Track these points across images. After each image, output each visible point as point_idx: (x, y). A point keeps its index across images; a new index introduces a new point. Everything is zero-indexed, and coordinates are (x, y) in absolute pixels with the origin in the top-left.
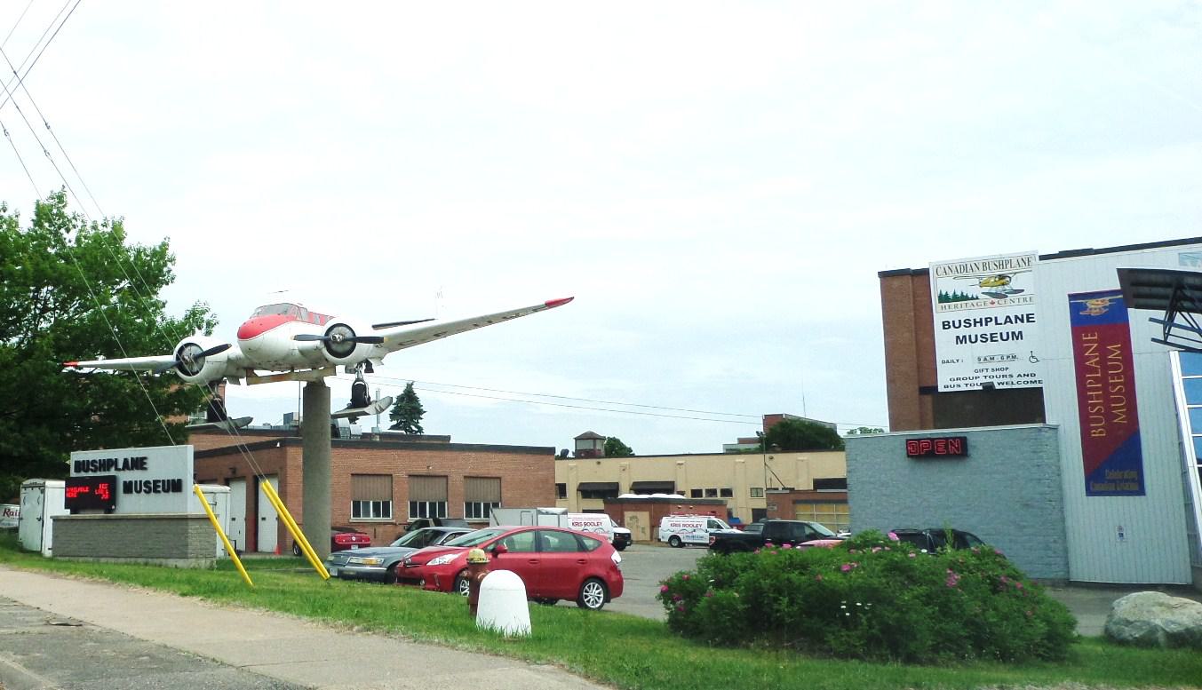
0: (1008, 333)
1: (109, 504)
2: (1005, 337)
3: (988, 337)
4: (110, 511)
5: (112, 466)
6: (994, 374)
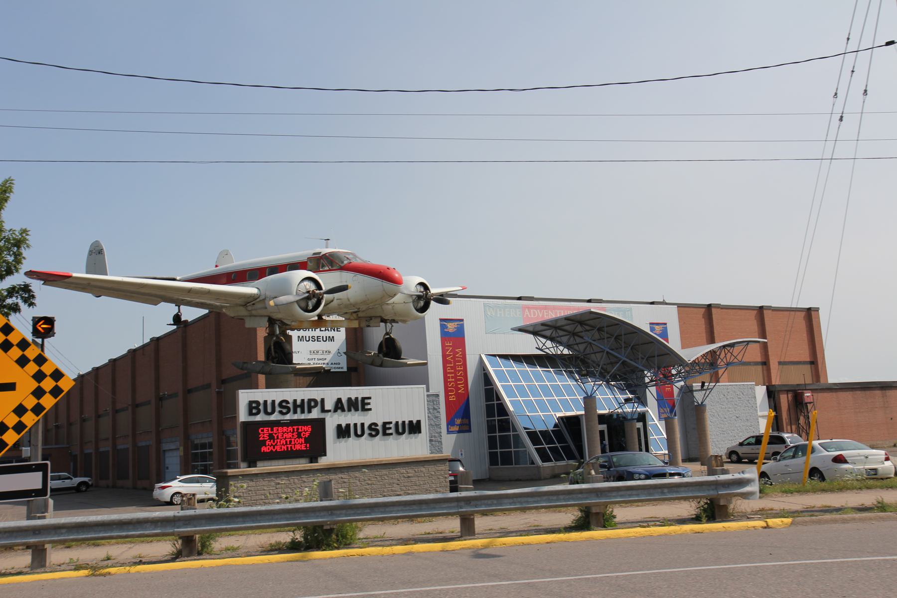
0: (326, 337)
1: (316, 448)
2: (325, 340)
3: (316, 338)
4: (314, 459)
5: (316, 406)
6: (319, 362)
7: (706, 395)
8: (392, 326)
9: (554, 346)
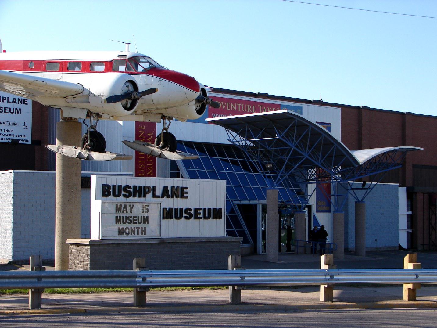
0: (13, 109)
2: (12, 111)
3: (3, 109)
5: (149, 192)
6: (5, 133)
7: (368, 192)
8: (170, 122)
9: (242, 140)
